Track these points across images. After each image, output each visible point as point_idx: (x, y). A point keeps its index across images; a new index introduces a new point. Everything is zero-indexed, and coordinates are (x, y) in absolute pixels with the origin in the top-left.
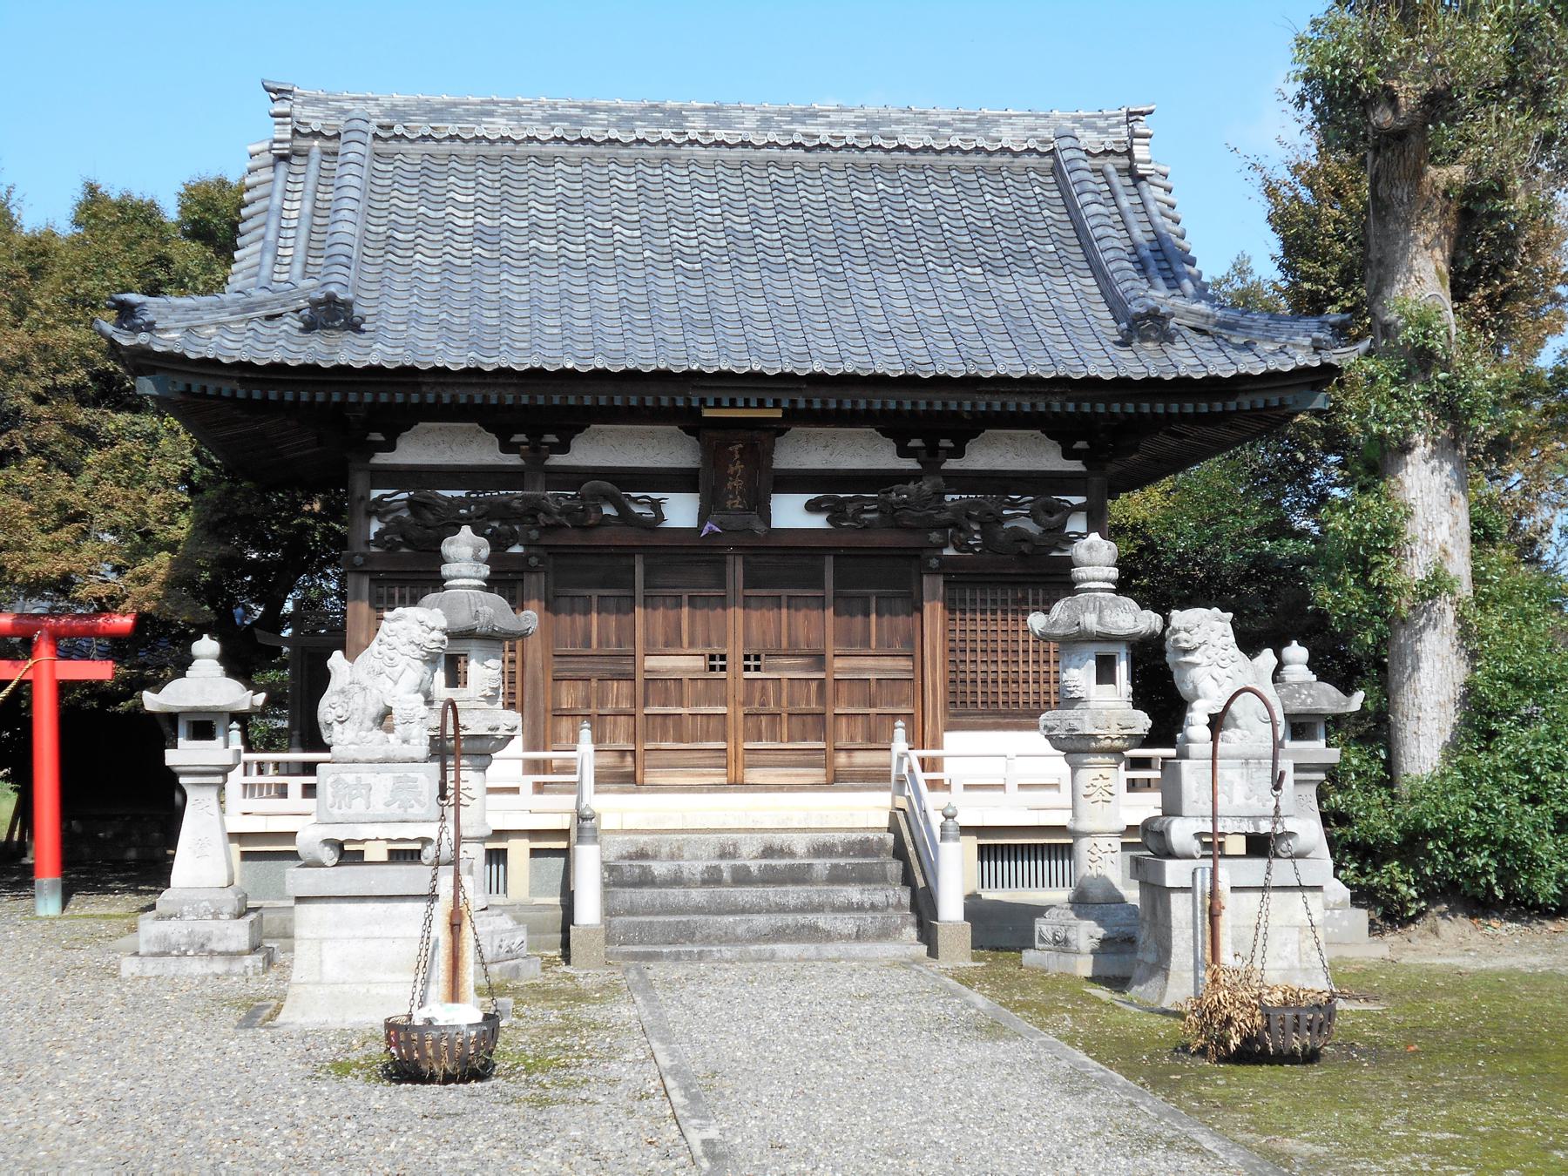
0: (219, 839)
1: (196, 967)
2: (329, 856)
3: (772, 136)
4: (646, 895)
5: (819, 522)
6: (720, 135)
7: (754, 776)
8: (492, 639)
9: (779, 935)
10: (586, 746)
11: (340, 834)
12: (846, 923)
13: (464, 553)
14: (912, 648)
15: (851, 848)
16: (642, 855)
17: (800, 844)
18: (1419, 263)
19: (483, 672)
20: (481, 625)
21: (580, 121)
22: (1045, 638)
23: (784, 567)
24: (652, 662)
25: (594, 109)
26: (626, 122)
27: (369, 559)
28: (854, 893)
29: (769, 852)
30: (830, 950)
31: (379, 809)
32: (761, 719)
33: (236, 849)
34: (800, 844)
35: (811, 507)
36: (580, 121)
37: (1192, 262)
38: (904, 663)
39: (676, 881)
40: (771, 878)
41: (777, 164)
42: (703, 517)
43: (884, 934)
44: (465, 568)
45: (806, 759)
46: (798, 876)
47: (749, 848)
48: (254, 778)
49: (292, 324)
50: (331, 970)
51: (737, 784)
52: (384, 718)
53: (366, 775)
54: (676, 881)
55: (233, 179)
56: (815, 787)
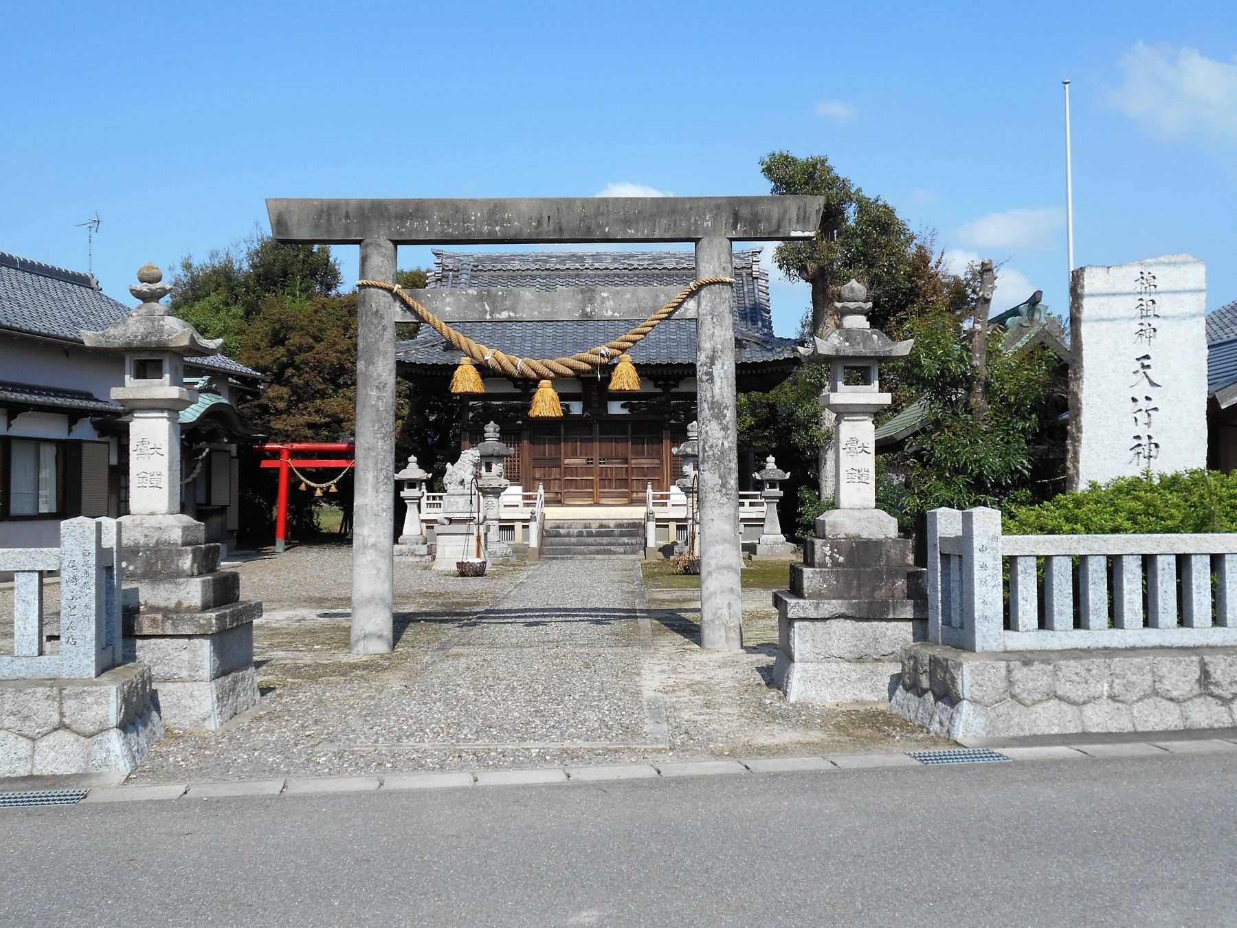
0: (418, 522)
1: (411, 559)
2: (446, 522)
3: (616, 266)
4: (557, 539)
5: (625, 411)
6: (597, 265)
7: (603, 501)
8: (499, 457)
9: (598, 552)
10: (541, 491)
11: (450, 516)
12: (621, 549)
13: (491, 429)
14: (659, 456)
15: (629, 525)
16: (558, 527)
17: (612, 524)
18: (828, 321)
19: (497, 468)
20: (495, 453)
21: (546, 262)
22: (677, 456)
23: (613, 428)
24: (567, 461)
25: (551, 257)
26: (563, 262)
27: (469, 426)
28: (626, 540)
29: (601, 526)
30: (613, 557)
31: (461, 509)
32: (605, 481)
33: (424, 525)
34: (612, 524)
35: (623, 406)
36: (546, 262)
37: (769, 312)
38: (656, 461)
39: (568, 535)
40: (599, 534)
41: (618, 276)
42: (584, 411)
43: (633, 552)
44: (491, 435)
45: (623, 495)
46: (609, 534)
47: (595, 525)
48: (431, 501)
49: (439, 348)
50: (447, 555)
51: (597, 504)
52: (462, 482)
53: (457, 499)
54: (568, 535)
55: (424, 269)
56: (625, 505)
